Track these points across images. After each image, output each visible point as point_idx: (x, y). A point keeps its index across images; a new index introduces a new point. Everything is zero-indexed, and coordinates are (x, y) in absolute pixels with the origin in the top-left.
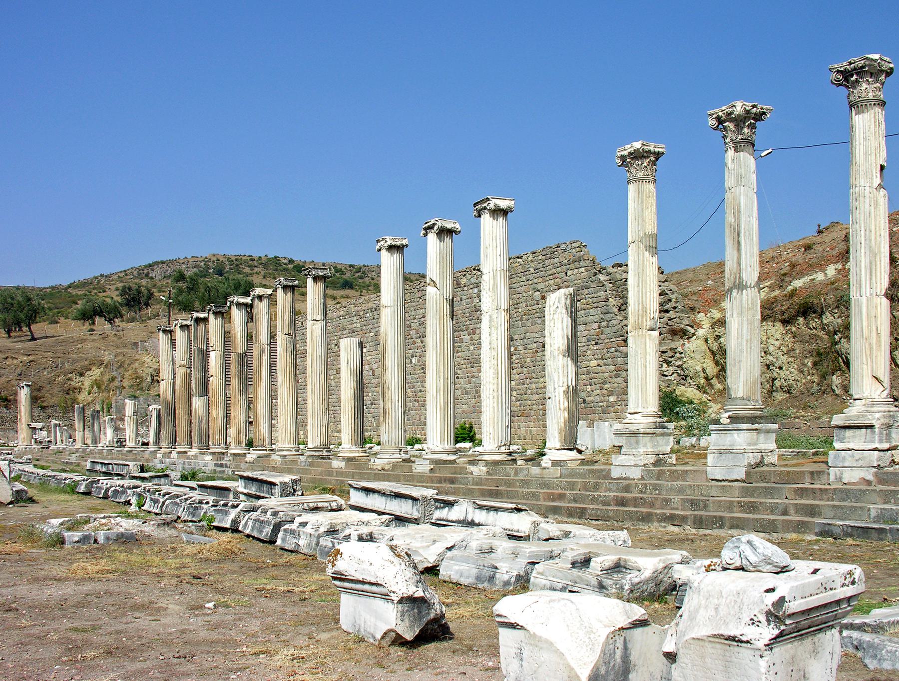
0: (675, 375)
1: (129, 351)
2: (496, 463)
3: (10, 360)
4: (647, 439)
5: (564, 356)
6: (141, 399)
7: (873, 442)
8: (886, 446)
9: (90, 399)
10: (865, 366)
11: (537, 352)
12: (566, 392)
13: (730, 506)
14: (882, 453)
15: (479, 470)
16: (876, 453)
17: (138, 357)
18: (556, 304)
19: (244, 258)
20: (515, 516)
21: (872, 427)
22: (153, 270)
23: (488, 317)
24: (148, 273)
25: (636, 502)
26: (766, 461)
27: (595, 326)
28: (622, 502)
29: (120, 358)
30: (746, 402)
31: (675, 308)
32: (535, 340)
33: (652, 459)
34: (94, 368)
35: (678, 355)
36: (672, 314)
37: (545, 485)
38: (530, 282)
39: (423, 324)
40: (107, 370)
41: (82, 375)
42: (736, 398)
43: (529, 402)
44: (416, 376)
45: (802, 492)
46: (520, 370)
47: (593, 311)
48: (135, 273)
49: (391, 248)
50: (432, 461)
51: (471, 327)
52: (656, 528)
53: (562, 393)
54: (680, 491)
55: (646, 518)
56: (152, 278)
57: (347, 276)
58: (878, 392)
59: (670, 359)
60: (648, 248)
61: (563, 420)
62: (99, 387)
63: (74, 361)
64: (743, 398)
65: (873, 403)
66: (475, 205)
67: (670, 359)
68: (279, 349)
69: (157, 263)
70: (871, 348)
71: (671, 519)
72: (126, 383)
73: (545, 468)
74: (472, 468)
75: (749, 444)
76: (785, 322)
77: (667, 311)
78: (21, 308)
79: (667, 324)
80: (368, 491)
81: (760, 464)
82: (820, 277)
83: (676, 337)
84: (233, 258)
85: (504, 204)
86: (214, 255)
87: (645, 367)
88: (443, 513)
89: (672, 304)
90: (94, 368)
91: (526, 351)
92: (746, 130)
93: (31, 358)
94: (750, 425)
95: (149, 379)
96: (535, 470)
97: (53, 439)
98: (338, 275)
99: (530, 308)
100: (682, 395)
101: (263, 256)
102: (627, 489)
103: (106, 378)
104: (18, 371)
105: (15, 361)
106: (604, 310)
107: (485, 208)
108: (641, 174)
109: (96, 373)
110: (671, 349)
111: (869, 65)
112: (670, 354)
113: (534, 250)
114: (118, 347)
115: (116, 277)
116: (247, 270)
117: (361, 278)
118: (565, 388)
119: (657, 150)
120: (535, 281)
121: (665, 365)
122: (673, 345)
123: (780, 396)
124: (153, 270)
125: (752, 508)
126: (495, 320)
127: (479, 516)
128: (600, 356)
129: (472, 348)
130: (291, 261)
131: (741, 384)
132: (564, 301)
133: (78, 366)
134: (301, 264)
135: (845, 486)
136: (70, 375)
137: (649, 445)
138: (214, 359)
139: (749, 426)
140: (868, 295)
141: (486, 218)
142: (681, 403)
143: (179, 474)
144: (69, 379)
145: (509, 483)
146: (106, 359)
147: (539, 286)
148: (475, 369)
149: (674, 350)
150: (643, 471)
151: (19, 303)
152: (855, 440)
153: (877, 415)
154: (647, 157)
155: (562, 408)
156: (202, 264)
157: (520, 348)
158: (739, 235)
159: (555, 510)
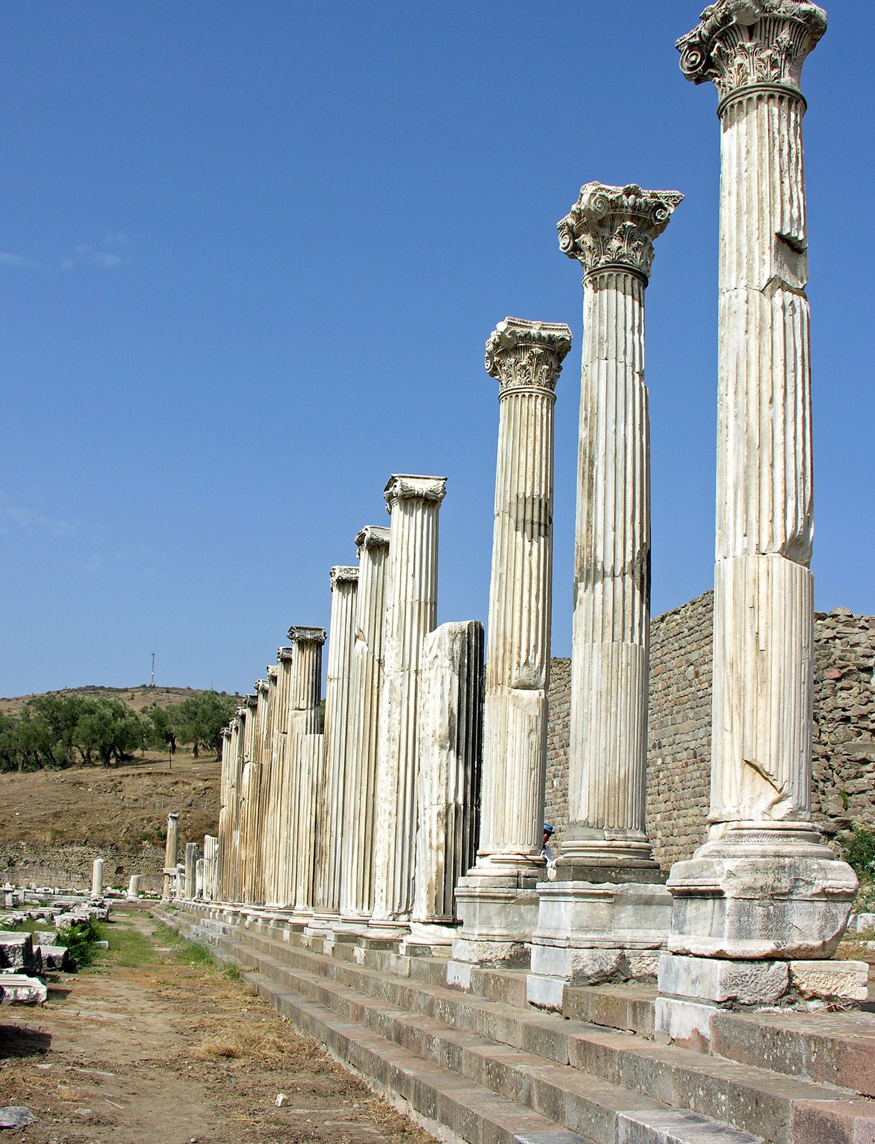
3: (181, 785)
5: (442, 747)
7: (720, 935)
8: (766, 946)
10: (727, 736)
11: (687, 765)
14: (743, 967)
16: (720, 963)
21: (718, 895)
26: (635, 968)
30: (592, 832)
32: (686, 745)
33: (503, 951)
38: (683, 651)
39: (566, 726)
42: (575, 824)
44: (557, 807)
58: (763, 804)
60: (521, 525)
61: (434, 869)
64: (586, 824)
65: (740, 834)
70: (741, 690)
75: (584, 928)
78: (206, 718)
85: (421, 486)
87: (504, 761)
91: (674, 765)
92: (615, 243)
93: (208, 784)
94: (587, 884)
99: (681, 693)
104: (188, 801)
105: (187, 788)
108: (516, 383)
113: (693, 599)
118: (441, 808)
119: (544, 333)
120: (689, 648)
126: (398, 689)
131: (585, 791)
135: (674, 1048)
137: (496, 921)
139: (583, 886)
140: (739, 553)
147: (693, 657)
150: (475, 974)
151: (204, 712)
153: (729, 864)
154: (526, 349)
155: (434, 845)
157: (669, 759)
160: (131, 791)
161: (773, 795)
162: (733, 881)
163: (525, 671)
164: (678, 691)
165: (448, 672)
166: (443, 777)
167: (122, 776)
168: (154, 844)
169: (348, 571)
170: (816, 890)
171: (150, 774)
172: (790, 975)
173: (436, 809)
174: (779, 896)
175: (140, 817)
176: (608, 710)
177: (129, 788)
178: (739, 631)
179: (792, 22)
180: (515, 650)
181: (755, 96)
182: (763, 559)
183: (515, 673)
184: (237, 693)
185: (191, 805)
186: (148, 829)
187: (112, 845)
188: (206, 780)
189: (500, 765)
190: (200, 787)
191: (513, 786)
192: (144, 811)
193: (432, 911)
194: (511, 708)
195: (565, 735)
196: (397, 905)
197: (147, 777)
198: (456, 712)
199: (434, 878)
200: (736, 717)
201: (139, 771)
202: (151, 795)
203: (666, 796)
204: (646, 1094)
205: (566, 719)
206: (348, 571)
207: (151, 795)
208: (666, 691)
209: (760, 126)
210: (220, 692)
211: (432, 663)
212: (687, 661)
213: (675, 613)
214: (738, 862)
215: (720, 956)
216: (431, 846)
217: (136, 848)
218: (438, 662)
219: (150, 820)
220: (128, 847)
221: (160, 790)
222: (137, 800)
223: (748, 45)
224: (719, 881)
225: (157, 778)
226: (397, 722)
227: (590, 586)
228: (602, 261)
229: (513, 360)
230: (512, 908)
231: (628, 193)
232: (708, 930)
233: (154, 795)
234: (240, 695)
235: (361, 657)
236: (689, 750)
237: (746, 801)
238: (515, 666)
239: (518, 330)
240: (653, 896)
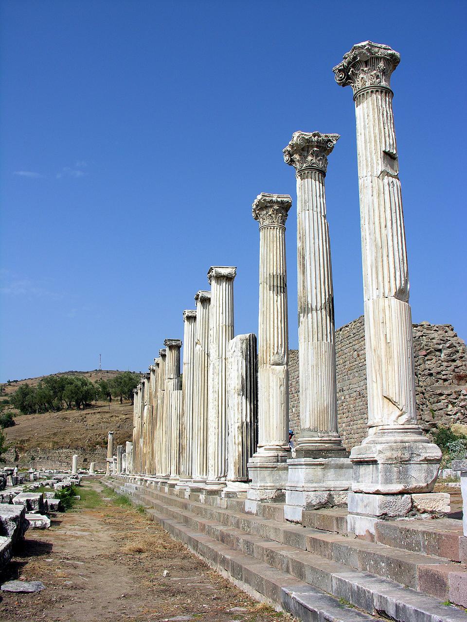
0: (459, 414)
4: (266, 473)
5: (239, 395)
8: (399, 487)
10: (375, 385)
21: (374, 462)
30: (312, 433)
31: (461, 357)
33: (272, 494)
35: (462, 397)
36: (458, 363)
38: (351, 345)
39: (298, 382)
42: (304, 430)
44: (295, 422)
46: (347, 414)
53: (236, 429)
54: (283, 527)
59: (454, 401)
61: (237, 454)
64: (309, 430)
65: (384, 432)
67: (454, 401)
70: (380, 362)
75: (311, 481)
77: (454, 361)
78: (126, 384)
79: (454, 371)
83: (462, 382)
85: (224, 271)
87: (269, 400)
89: (459, 355)
91: (350, 399)
100: (456, 431)
104: (118, 425)
108: (267, 222)
110: (455, 392)
111: (360, 54)
112: (454, 396)
118: (240, 424)
119: (279, 200)
121: (450, 406)
126: (217, 367)
132: (240, 346)
135: (357, 540)
137: (268, 479)
139: (309, 460)
140: (375, 297)
142: (454, 438)
143: (54, 494)
147: (356, 347)
150: (259, 506)
153: (379, 447)
154: (271, 207)
155: (237, 443)
157: (347, 397)
158: (304, 258)
162: (382, 455)
165: (241, 358)
166: (240, 409)
168: (102, 447)
170: (422, 458)
171: (99, 412)
172: (412, 501)
173: (237, 425)
174: (404, 462)
176: (317, 374)
179: (384, 58)
180: (272, 347)
181: (370, 91)
183: (272, 358)
186: (99, 439)
188: (126, 415)
190: (123, 418)
192: (97, 431)
194: (271, 374)
196: (219, 473)
201: (94, 411)
202: (100, 423)
207: (100, 423)
209: (373, 104)
213: (346, 327)
215: (377, 493)
217: (93, 449)
218: (235, 354)
219: (100, 435)
220: (89, 449)
222: (93, 425)
224: (375, 455)
225: (103, 414)
228: (304, 166)
230: (275, 472)
231: (314, 135)
232: (371, 480)
235: (199, 352)
236: (357, 392)
237: (386, 416)
238: (272, 354)
239: (267, 198)
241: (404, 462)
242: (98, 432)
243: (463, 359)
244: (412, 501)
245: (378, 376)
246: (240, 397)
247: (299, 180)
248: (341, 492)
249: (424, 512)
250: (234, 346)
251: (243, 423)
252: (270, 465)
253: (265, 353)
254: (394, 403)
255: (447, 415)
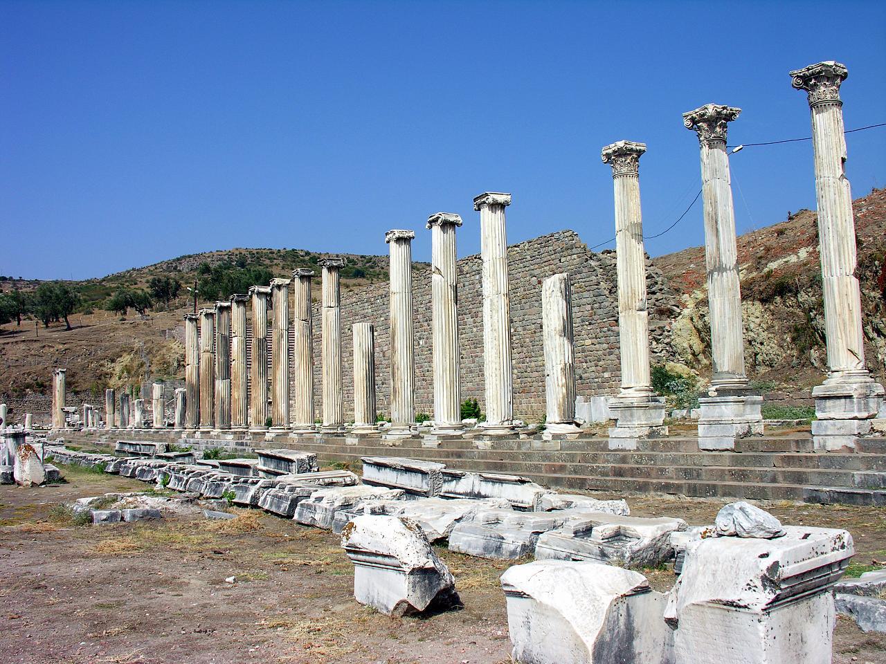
0: (664, 351)
1: (158, 338)
2: (500, 437)
4: (641, 411)
5: (560, 336)
6: (168, 383)
7: (853, 411)
9: (120, 383)
10: (840, 341)
12: (564, 370)
13: (722, 474)
14: (861, 422)
15: (484, 445)
17: (165, 344)
18: (552, 287)
19: (264, 251)
20: (519, 487)
21: (850, 397)
22: (181, 264)
23: (489, 300)
24: (176, 266)
25: (632, 472)
26: (753, 431)
27: (589, 307)
28: (619, 473)
29: (149, 345)
30: (732, 376)
31: (661, 290)
32: (534, 321)
33: (646, 431)
34: (125, 355)
35: (666, 333)
36: (658, 295)
37: (547, 457)
40: (137, 356)
41: (113, 361)
43: (529, 379)
44: (423, 357)
45: (789, 460)
47: (586, 294)
48: (164, 267)
49: (399, 240)
50: (440, 437)
51: (474, 310)
52: (652, 497)
53: (559, 371)
55: (643, 488)
56: (180, 271)
57: (359, 266)
58: (854, 364)
62: (129, 372)
63: (106, 349)
64: (728, 372)
66: (475, 200)
68: (296, 334)
69: (184, 257)
71: (666, 488)
72: (154, 368)
73: (546, 441)
74: (478, 443)
75: (737, 415)
76: (763, 301)
77: (654, 293)
78: (58, 299)
80: (380, 466)
81: (748, 433)
82: (793, 259)
84: (255, 252)
85: (501, 198)
86: (237, 249)
87: (636, 344)
88: (451, 486)
90: (125, 355)
92: (718, 129)
93: (67, 346)
95: (176, 364)
96: (537, 444)
97: (84, 422)
98: (350, 265)
101: (281, 249)
102: (624, 460)
103: (136, 363)
104: (54, 359)
106: (595, 293)
107: (484, 202)
108: (624, 170)
109: (126, 359)
110: (659, 328)
111: (826, 71)
114: (147, 335)
115: (147, 270)
116: (267, 262)
117: (372, 267)
118: (562, 366)
119: (638, 148)
122: (661, 324)
123: (762, 370)
124: (181, 264)
125: (743, 476)
126: (496, 304)
127: (485, 488)
128: (594, 335)
129: (475, 329)
130: (308, 253)
131: (726, 359)
132: (558, 286)
133: (110, 353)
134: (317, 255)
136: (102, 362)
138: (236, 344)
141: (485, 211)
142: (671, 378)
144: (101, 366)
145: (513, 457)
146: (136, 346)
147: (536, 272)
148: (478, 350)
149: (661, 328)
150: (638, 442)
152: (835, 410)
153: (855, 386)
154: (630, 155)
156: (226, 257)
159: (557, 482)
160: (13, 354)
161: (858, 361)
162: (856, 392)
163: (641, 302)
164: (525, 290)
165: (561, 298)
166: (562, 350)
167: (4, 344)
168: (34, 391)
169: (401, 232)
170: (876, 394)
171: (24, 341)
172: (872, 424)
173: (560, 367)
174: (867, 397)
175: (22, 372)
176: (733, 326)
177: (10, 352)
178: (841, 303)
179: (841, 75)
180: (637, 294)
181: (831, 104)
182: (848, 278)
183: (638, 304)
184: (20, 277)
185: (56, 362)
186: (29, 380)
187: (4, 394)
188: (65, 344)
189: (635, 346)
190: (61, 349)
191: (641, 355)
192: (24, 368)
193: (561, 417)
194: (637, 319)
195: (429, 314)
196: (503, 417)
197: (22, 344)
198: (565, 319)
199: (561, 400)
200: (843, 333)
201: (15, 340)
202: (27, 356)
203: (520, 350)
204: (291, 540)
205: (429, 304)
206: (401, 232)
207: (27, 356)
208: (514, 290)
209: (833, 115)
210: (8, 277)
211: (551, 294)
212: (531, 275)
213: (515, 246)
214: (857, 385)
215: (855, 418)
216: (558, 385)
217: (22, 395)
218: (554, 294)
219: (29, 374)
220: (15, 394)
221: (33, 352)
222: (17, 360)
223: (827, 83)
224: (851, 392)
225: (29, 344)
226: (496, 321)
227: (720, 274)
228: (713, 136)
229: (624, 159)
230: (647, 411)
231: (724, 108)
232: (843, 410)
233: (29, 356)
234: (23, 279)
235: (440, 284)
236: (536, 324)
237: (849, 363)
238: (637, 301)
239: (628, 146)
240: (755, 401)
241: (867, 397)
242: (26, 369)
243: (663, 292)
244: (872, 424)
245: (843, 333)
246: (562, 338)
247: (705, 150)
248: (756, 424)
249: (877, 432)
250: (552, 285)
251: (566, 365)
252: (644, 404)
253: (630, 299)
254: (854, 354)
255: (654, 352)
